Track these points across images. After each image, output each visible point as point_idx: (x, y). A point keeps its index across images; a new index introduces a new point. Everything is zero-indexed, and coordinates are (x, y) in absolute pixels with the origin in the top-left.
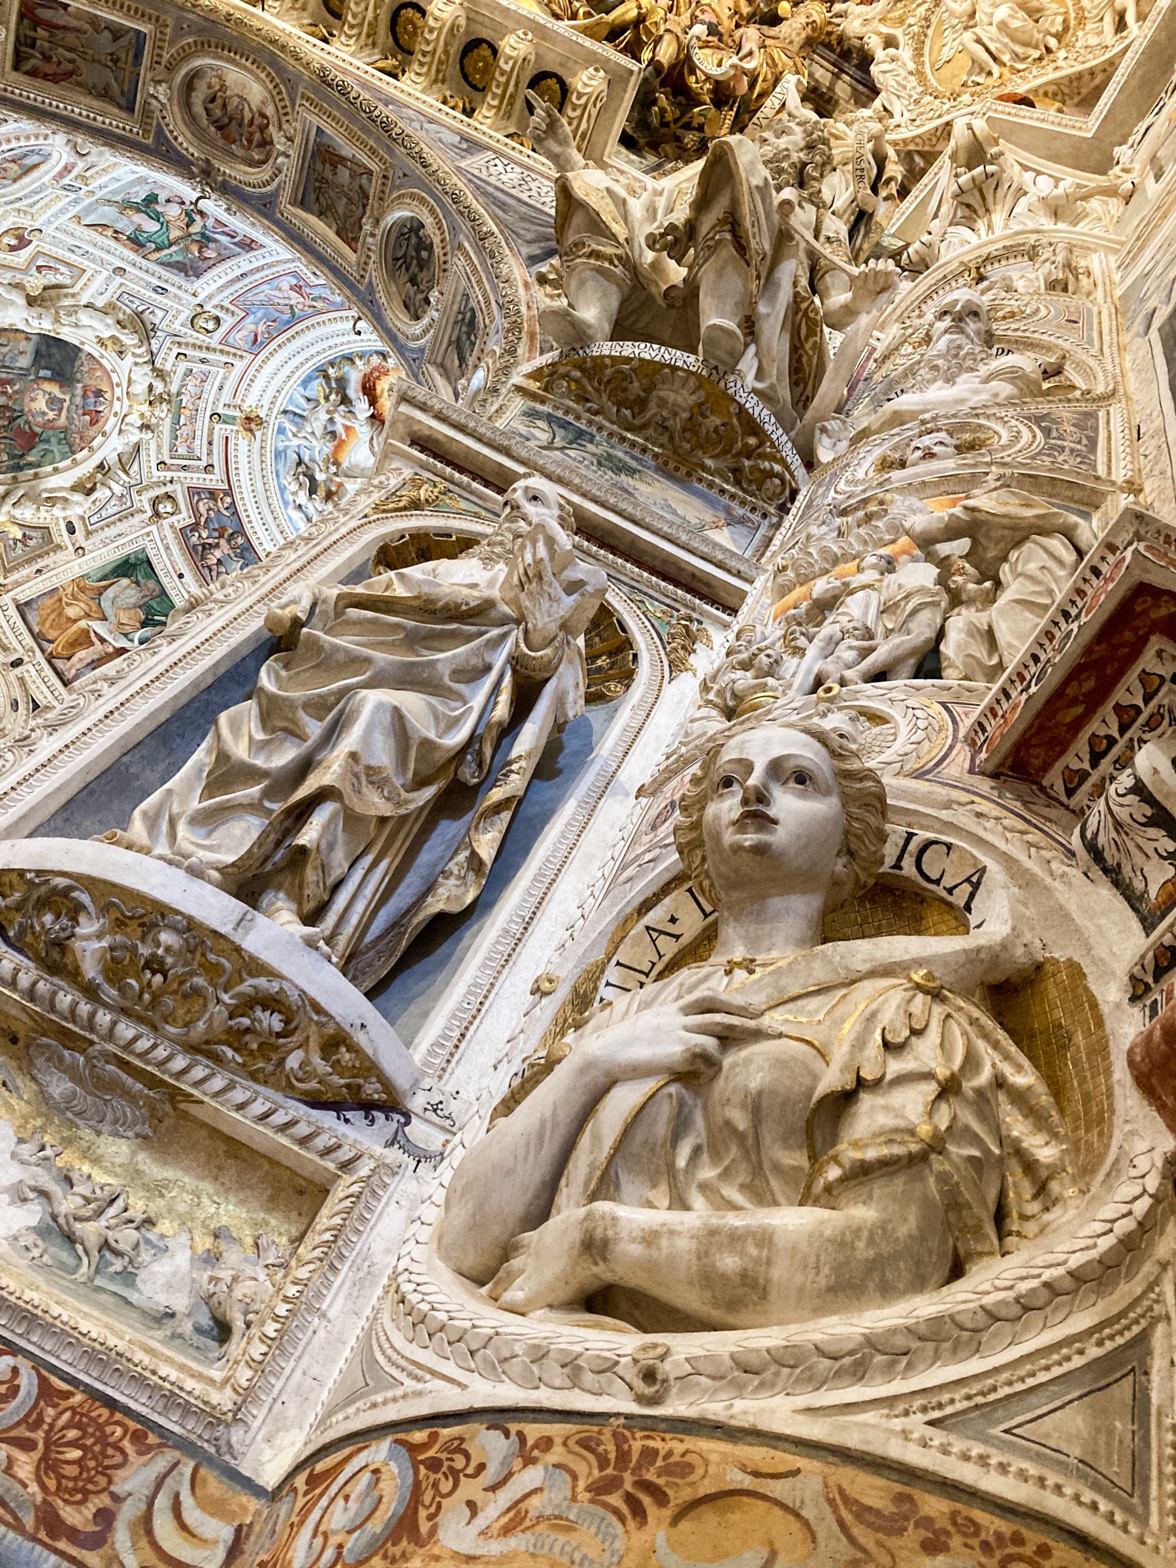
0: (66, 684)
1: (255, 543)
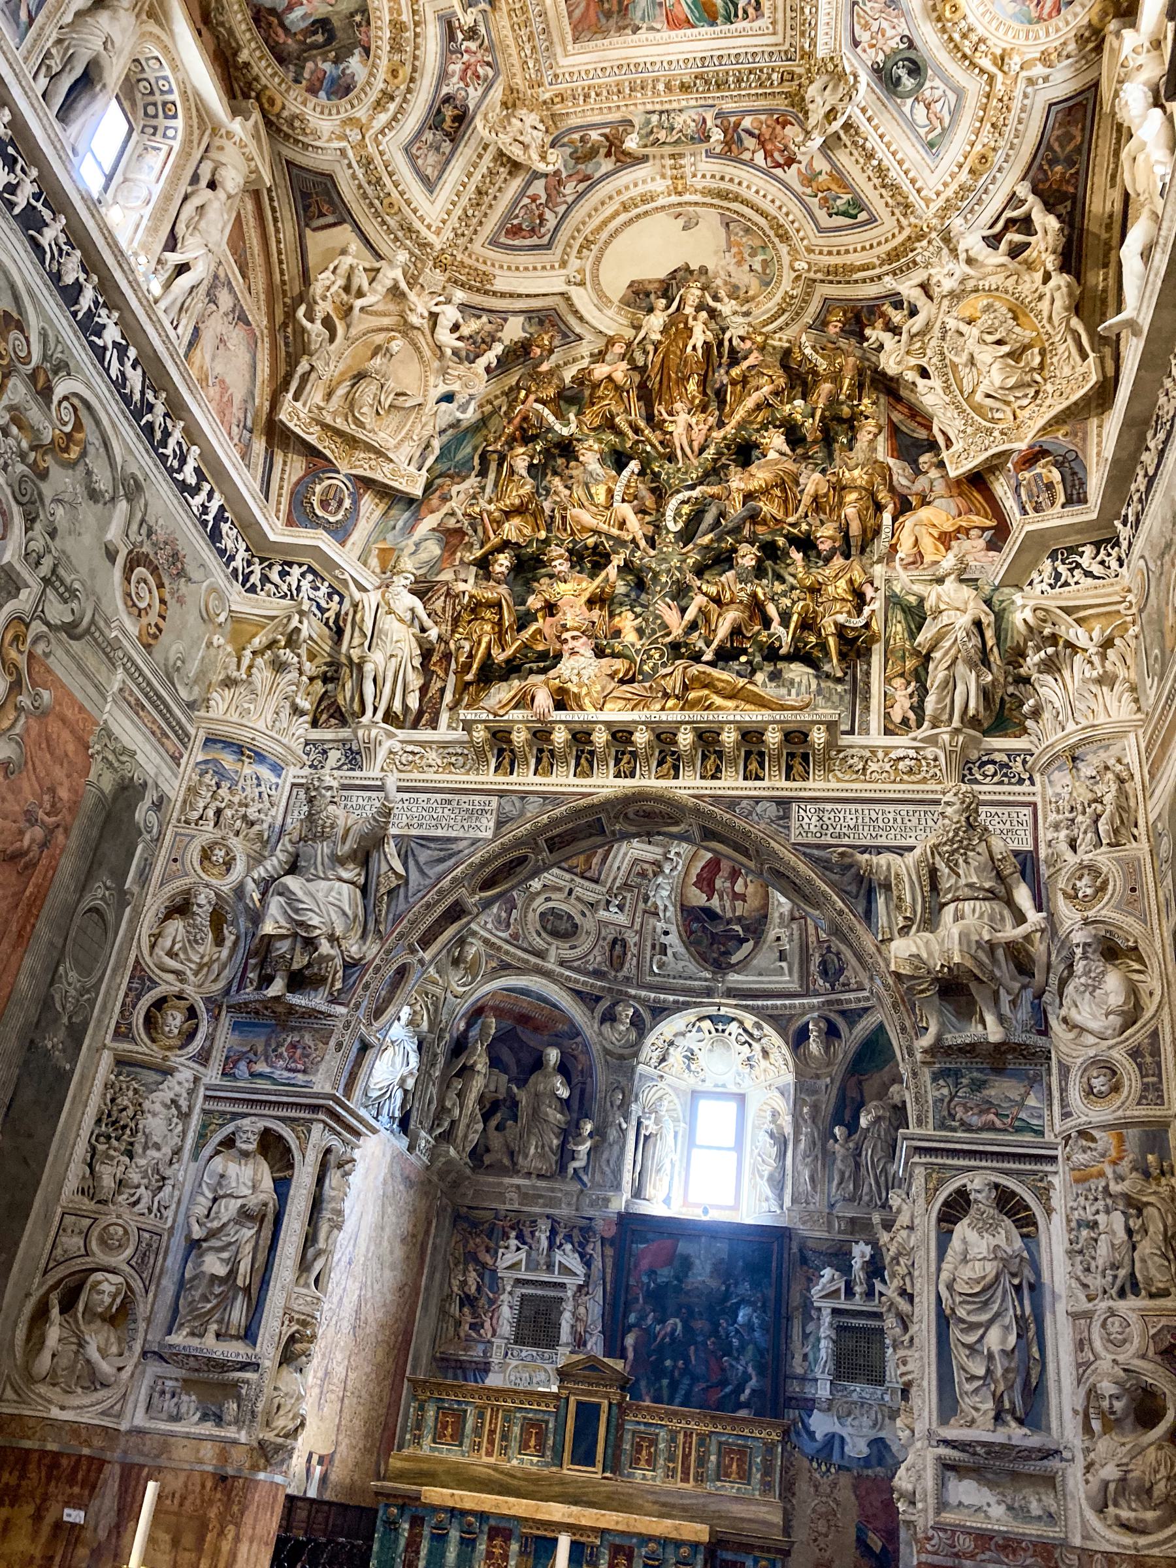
0: (596, 882)
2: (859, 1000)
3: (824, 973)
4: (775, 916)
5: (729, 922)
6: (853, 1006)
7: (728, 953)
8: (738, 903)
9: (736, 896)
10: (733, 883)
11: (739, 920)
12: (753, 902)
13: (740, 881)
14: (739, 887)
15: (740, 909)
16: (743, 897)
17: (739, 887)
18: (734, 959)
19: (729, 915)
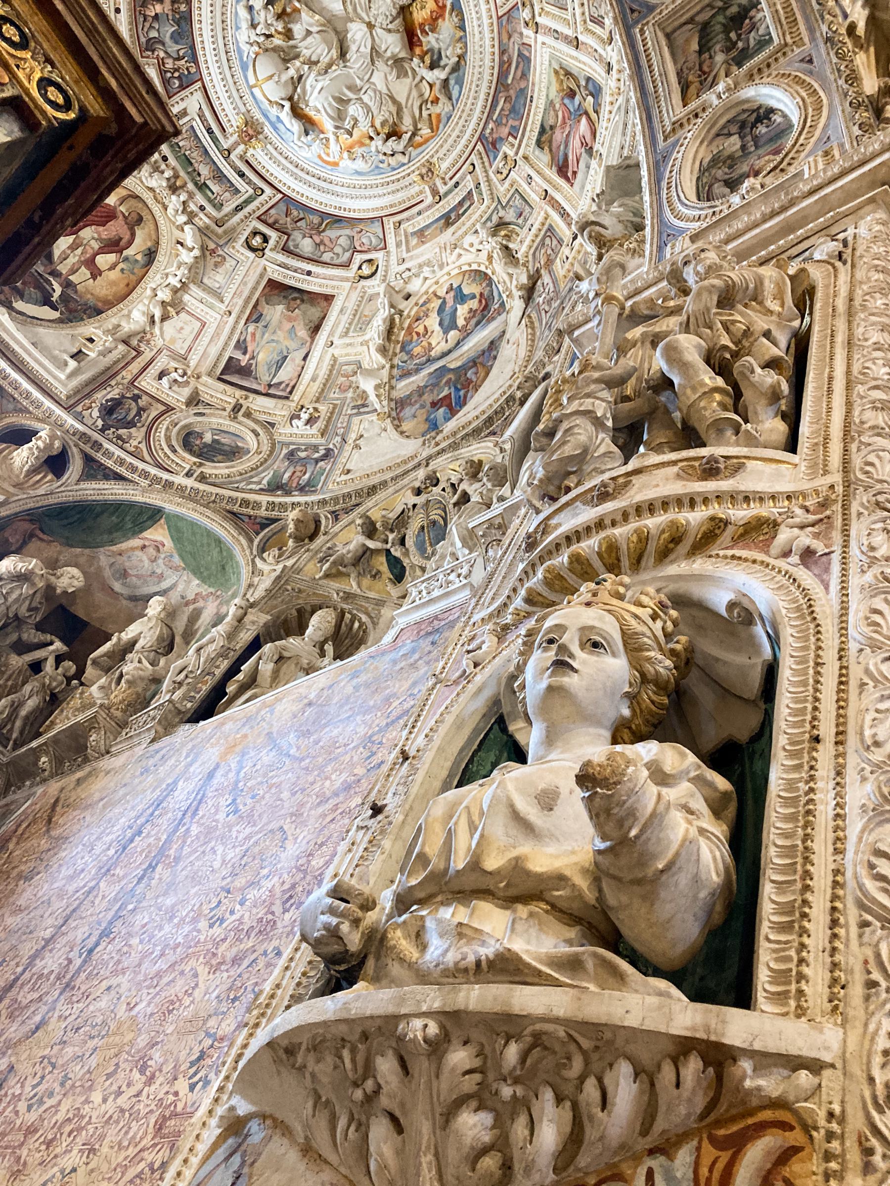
1: (195, 18)
2: (122, 462)
3: (110, 409)
4: (111, 318)
5: (55, 274)
6: (109, 463)
7: (21, 296)
8: (85, 273)
9: (90, 263)
10: (102, 251)
11: (68, 285)
12: (100, 288)
13: (112, 257)
14: (104, 260)
15: (81, 276)
16: (96, 273)
17: (104, 260)
18: (19, 305)
19: (63, 268)
